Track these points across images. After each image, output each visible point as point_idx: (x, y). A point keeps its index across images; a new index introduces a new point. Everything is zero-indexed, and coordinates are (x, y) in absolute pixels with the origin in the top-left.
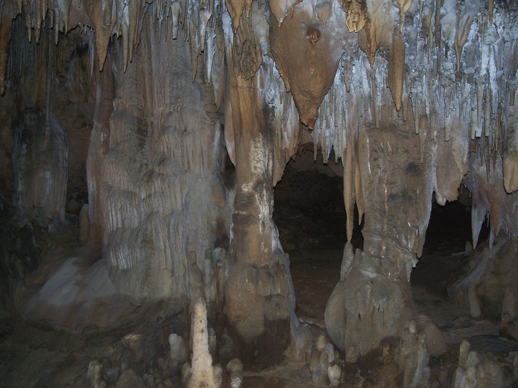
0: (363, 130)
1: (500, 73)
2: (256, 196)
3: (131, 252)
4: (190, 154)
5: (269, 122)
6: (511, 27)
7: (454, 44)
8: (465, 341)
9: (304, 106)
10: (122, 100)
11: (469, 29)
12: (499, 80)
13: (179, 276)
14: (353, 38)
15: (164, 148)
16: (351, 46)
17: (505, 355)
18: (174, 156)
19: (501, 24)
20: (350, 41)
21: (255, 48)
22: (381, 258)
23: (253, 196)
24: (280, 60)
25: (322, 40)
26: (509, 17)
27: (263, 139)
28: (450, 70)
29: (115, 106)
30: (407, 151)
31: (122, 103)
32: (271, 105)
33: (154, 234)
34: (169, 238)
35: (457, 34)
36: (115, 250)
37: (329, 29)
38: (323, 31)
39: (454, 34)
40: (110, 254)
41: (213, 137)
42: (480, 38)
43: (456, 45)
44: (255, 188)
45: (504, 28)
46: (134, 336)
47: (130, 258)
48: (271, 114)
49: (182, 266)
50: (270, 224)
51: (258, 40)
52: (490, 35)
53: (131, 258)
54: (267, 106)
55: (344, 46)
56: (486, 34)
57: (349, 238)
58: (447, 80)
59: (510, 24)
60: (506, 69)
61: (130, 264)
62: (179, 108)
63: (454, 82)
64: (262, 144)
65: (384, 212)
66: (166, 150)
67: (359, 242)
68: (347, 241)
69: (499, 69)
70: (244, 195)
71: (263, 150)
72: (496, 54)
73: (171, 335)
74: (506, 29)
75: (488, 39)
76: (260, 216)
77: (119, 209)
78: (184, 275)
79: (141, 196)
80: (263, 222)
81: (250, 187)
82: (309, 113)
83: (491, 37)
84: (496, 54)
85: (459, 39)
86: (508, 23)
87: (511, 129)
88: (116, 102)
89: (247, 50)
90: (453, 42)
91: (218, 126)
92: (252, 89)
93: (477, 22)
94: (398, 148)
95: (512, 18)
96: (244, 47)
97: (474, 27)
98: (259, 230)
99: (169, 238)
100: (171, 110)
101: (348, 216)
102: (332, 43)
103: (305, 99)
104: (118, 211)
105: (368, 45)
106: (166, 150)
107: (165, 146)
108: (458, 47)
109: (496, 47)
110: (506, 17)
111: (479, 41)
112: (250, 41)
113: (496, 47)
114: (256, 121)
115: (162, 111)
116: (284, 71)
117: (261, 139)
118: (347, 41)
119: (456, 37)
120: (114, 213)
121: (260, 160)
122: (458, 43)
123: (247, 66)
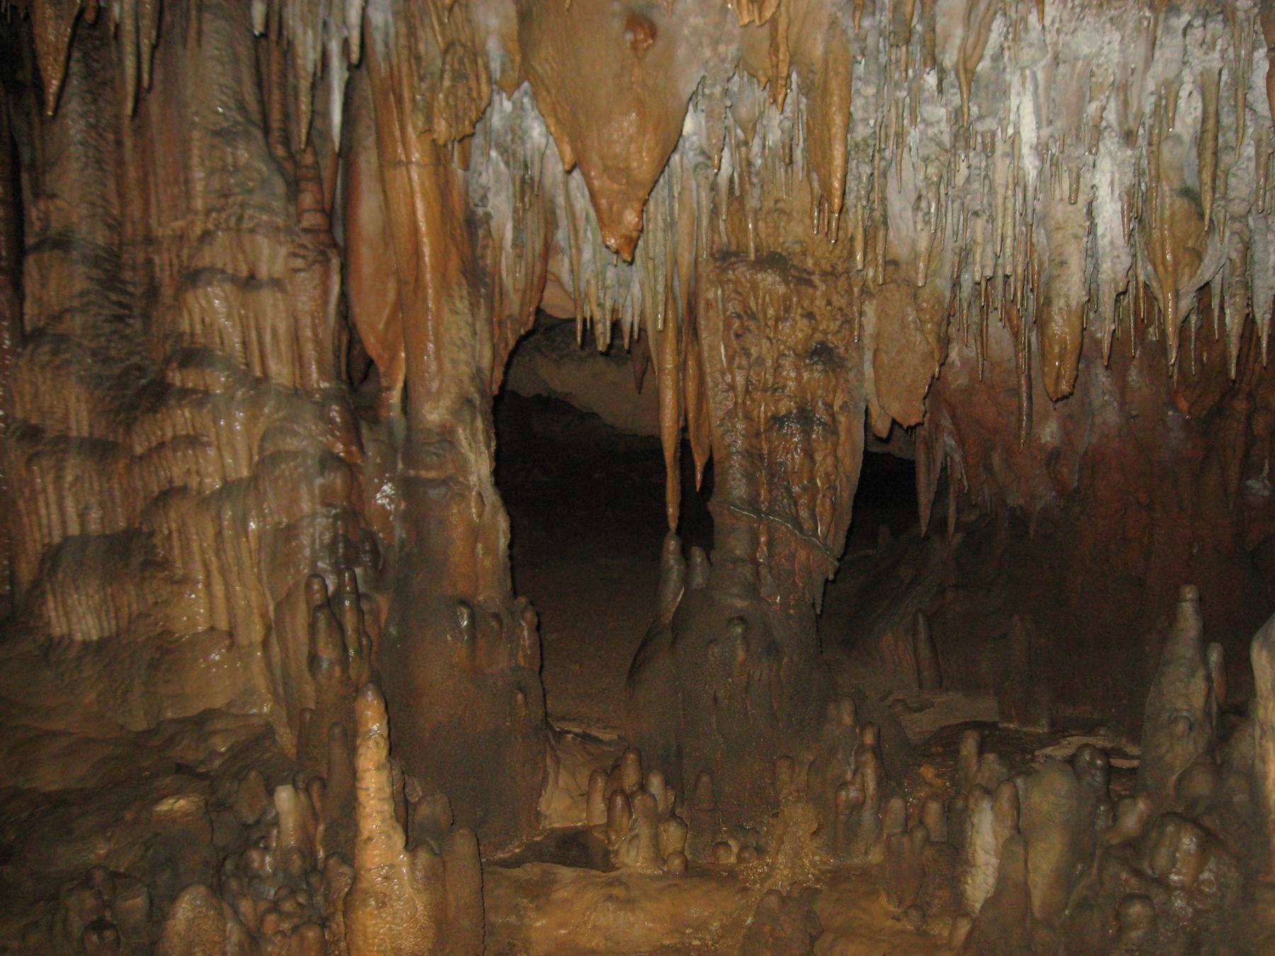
0: (707, 270)
1: (1046, 132)
2: (460, 431)
3: (113, 595)
4: (268, 338)
5: (479, 251)
6: (1075, 30)
7: (958, 62)
8: (969, 732)
9: (611, 205)
10: (59, 202)
11: (989, 30)
12: (1041, 150)
13: (250, 645)
14: (729, 42)
15: (192, 325)
16: (723, 61)
17: (1029, 757)
18: (222, 344)
19: (1053, 22)
20: (722, 48)
21: (476, 62)
22: (758, 564)
23: (452, 431)
24: (549, 92)
25: (661, 44)
26: (1073, 8)
27: (469, 293)
28: (938, 122)
29: (39, 219)
30: (810, 316)
31: (59, 210)
32: (480, 211)
33: (176, 543)
34: (219, 551)
35: (965, 40)
36: (62, 593)
37: (674, 19)
38: (662, 21)
39: (958, 41)
40: (44, 603)
41: (326, 292)
42: (1007, 54)
43: (961, 67)
44: (456, 413)
45: (1058, 31)
46: (182, 802)
47: (107, 611)
48: (481, 232)
49: (257, 619)
50: (492, 497)
51: (484, 44)
52: (1031, 45)
53: (112, 610)
54: (473, 213)
55: (707, 62)
56: (1023, 44)
57: (673, 525)
58: (933, 144)
59: (1073, 23)
60: (1059, 124)
61: (110, 627)
62: (233, 220)
63: (946, 151)
64: (466, 303)
65: (761, 456)
66: (198, 328)
67: (699, 527)
68: (667, 528)
69: (1044, 123)
70: (429, 431)
71: (470, 320)
72: (1041, 91)
73: (280, 788)
74: (1062, 36)
75: (1027, 54)
76: (473, 479)
77: (67, 485)
78: (265, 644)
79: (131, 447)
80: (480, 494)
81: (443, 411)
82: (620, 222)
83: (1033, 50)
84: (1041, 91)
85: (969, 51)
86: (1070, 21)
87: (1058, 259)
88: (42, 207)
89: (456, 66)
90: (955, 58)
91: (335, 263)
92: (441, 169)
93: (1005, 14)
94: (790, 306)
95: (1078, 10)
96: (449, 58)
97: (998, 25)
98: (471, 514)
99: (219, 551)
100: (211, 226)
101: (669, 471)
102: (682, 52)
103: (615, 186)
104: (66, 493)
105: (774, 59)
106: (198, 328)
107: (197, 318)
108: (966, 70)
109: (1040, 76)
110: (1065, 6)
111: (1006, 58)
112: (464, 46)
113: (1040, 76)
114: (453, 250)
115: (182, 229)
116: (558, 121)
117: (465, 293)
118: (714, 50)
119: (963, 48)
120: (52, 497)
121: (464, 344)
122: (965, 62)
123: (456, 106)
